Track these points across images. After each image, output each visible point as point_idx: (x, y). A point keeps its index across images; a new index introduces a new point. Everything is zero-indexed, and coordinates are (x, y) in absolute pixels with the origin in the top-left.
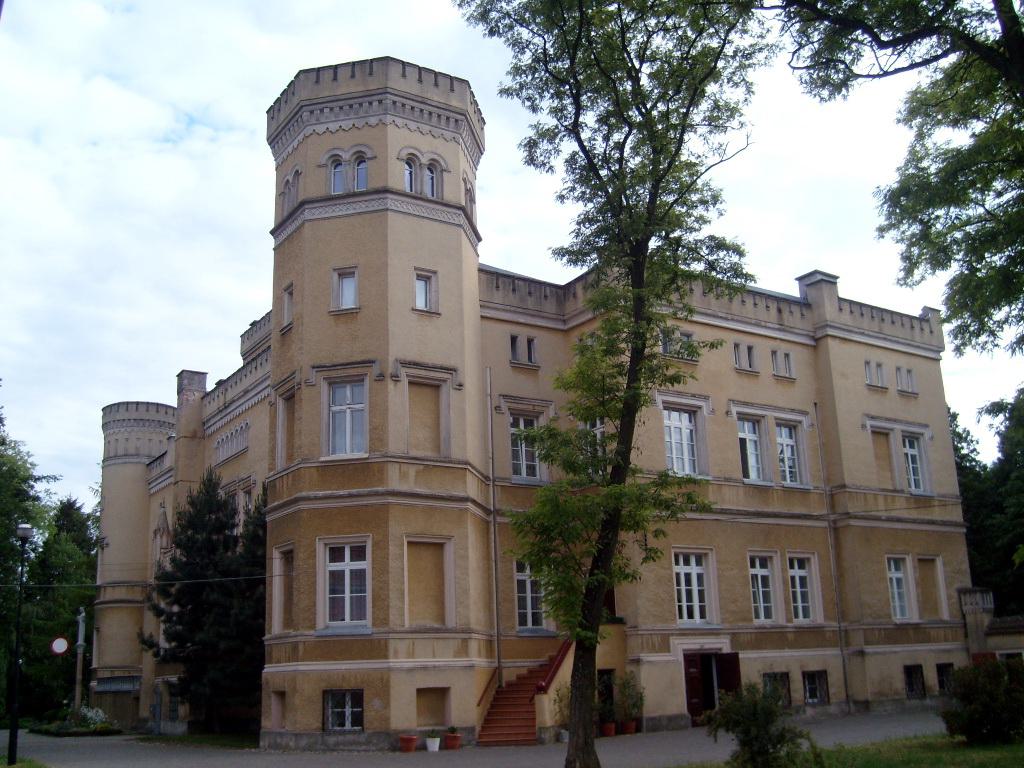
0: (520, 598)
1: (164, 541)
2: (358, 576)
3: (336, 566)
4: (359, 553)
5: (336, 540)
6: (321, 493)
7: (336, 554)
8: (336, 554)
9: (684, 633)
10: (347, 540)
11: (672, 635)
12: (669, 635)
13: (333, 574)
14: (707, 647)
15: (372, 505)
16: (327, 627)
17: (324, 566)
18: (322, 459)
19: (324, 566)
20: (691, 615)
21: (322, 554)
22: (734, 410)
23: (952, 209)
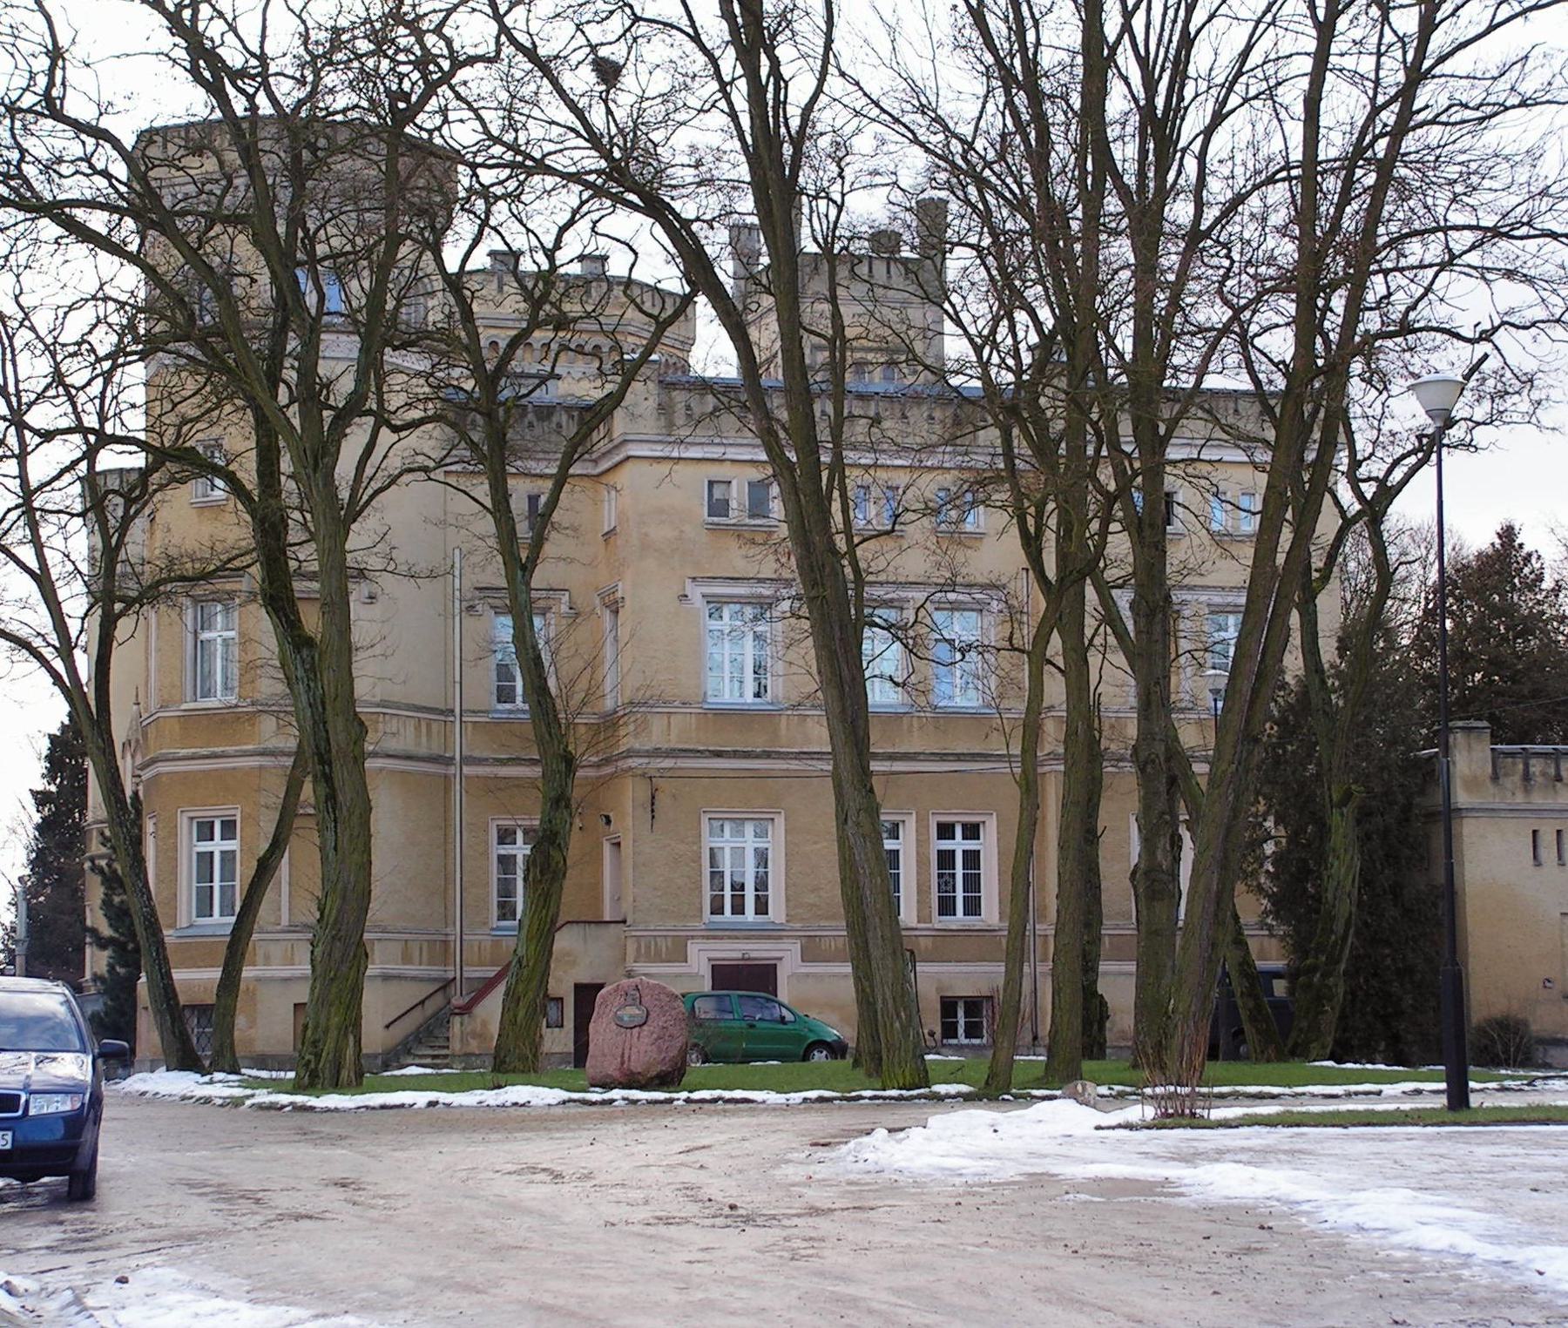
0: (713, 898)
1: (1474, 745)
2: (972, 858)
3: (205, 847)
4: (229, 829)
5: (204, 813)
6: (183, 752)
7: (206, 832)
8: (206, 832)
9: (714, 934)
10: (216, 814)
11: (693, 937)
12: (688, 938)
13: (501, 859)
14: (753, 955)
15: (241, 769)
16: (191, 926)
17: (190, 847)
18: (184, 706)
19: (190, 847)
20: (738, 909)
21: (185, 830)
22: (696, 592)
23: (291, 539)
